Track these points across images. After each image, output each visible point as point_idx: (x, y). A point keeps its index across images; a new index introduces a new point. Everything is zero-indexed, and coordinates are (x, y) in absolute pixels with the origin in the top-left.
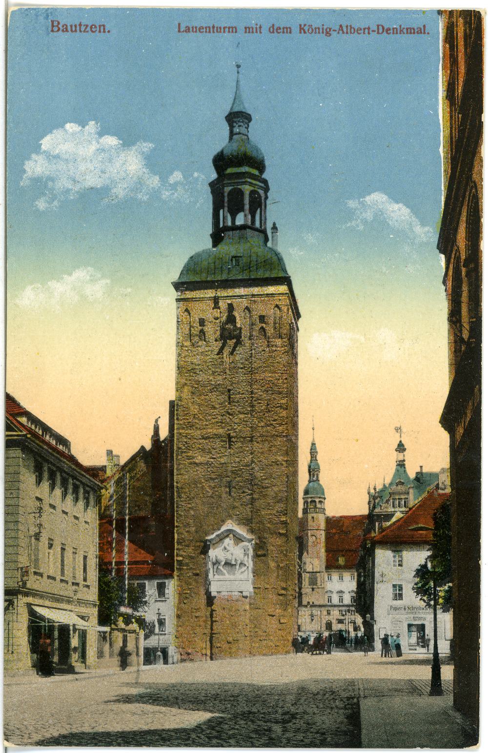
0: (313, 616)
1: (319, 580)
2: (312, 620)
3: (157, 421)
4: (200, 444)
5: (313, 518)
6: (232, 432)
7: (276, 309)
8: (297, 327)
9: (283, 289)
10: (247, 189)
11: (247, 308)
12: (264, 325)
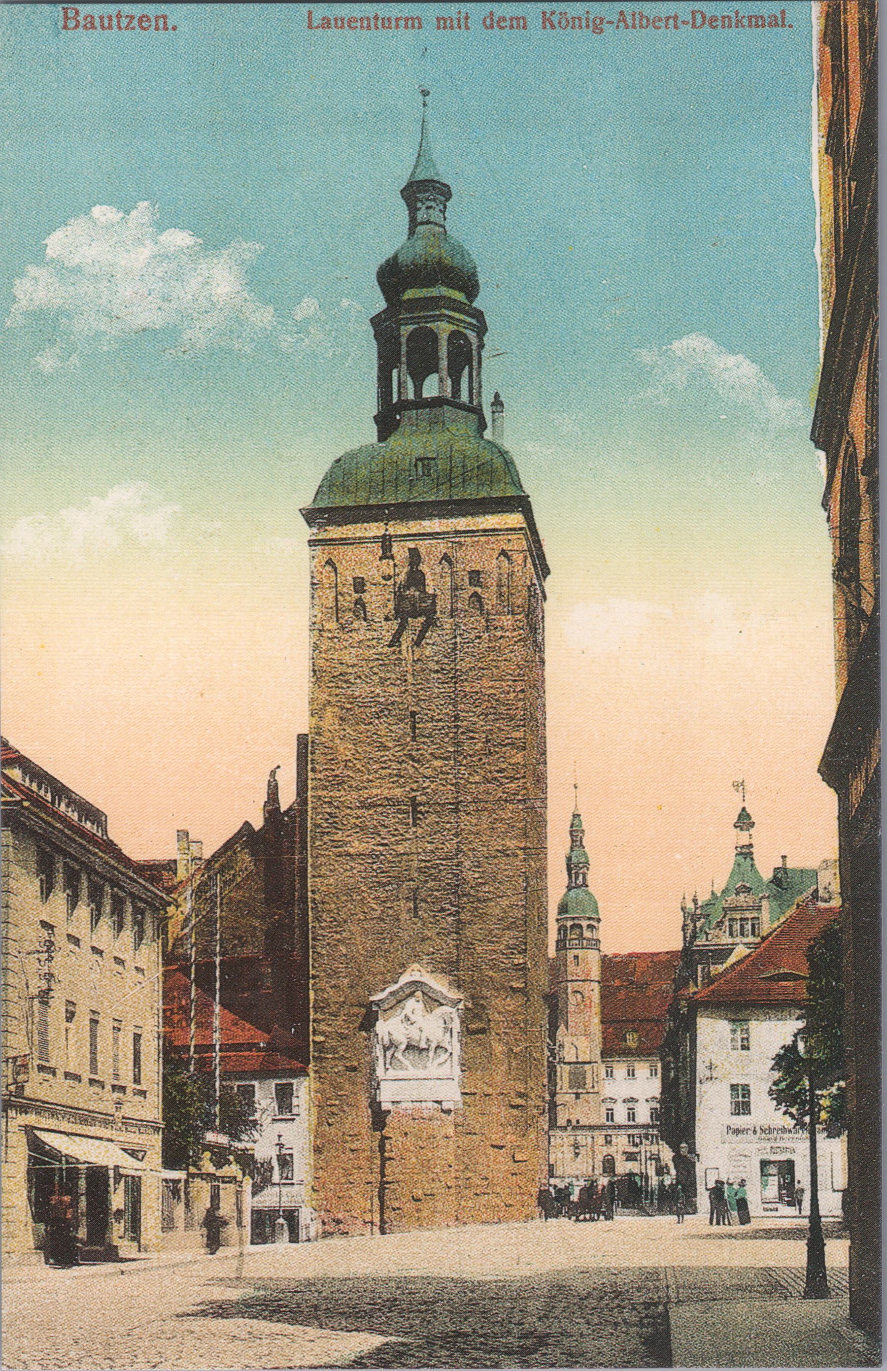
0: (577, 1148)
1: (589, 1075)
2: (577, 1154)
3: (273, 773)
4: (357, 818)
5: (576, 957)
6: (419, 793)
7: (502, 558)
8: (543, 592)
9: (515, 519)
10: (444, 329)
11: (446, 557)
12: (479, 590)
